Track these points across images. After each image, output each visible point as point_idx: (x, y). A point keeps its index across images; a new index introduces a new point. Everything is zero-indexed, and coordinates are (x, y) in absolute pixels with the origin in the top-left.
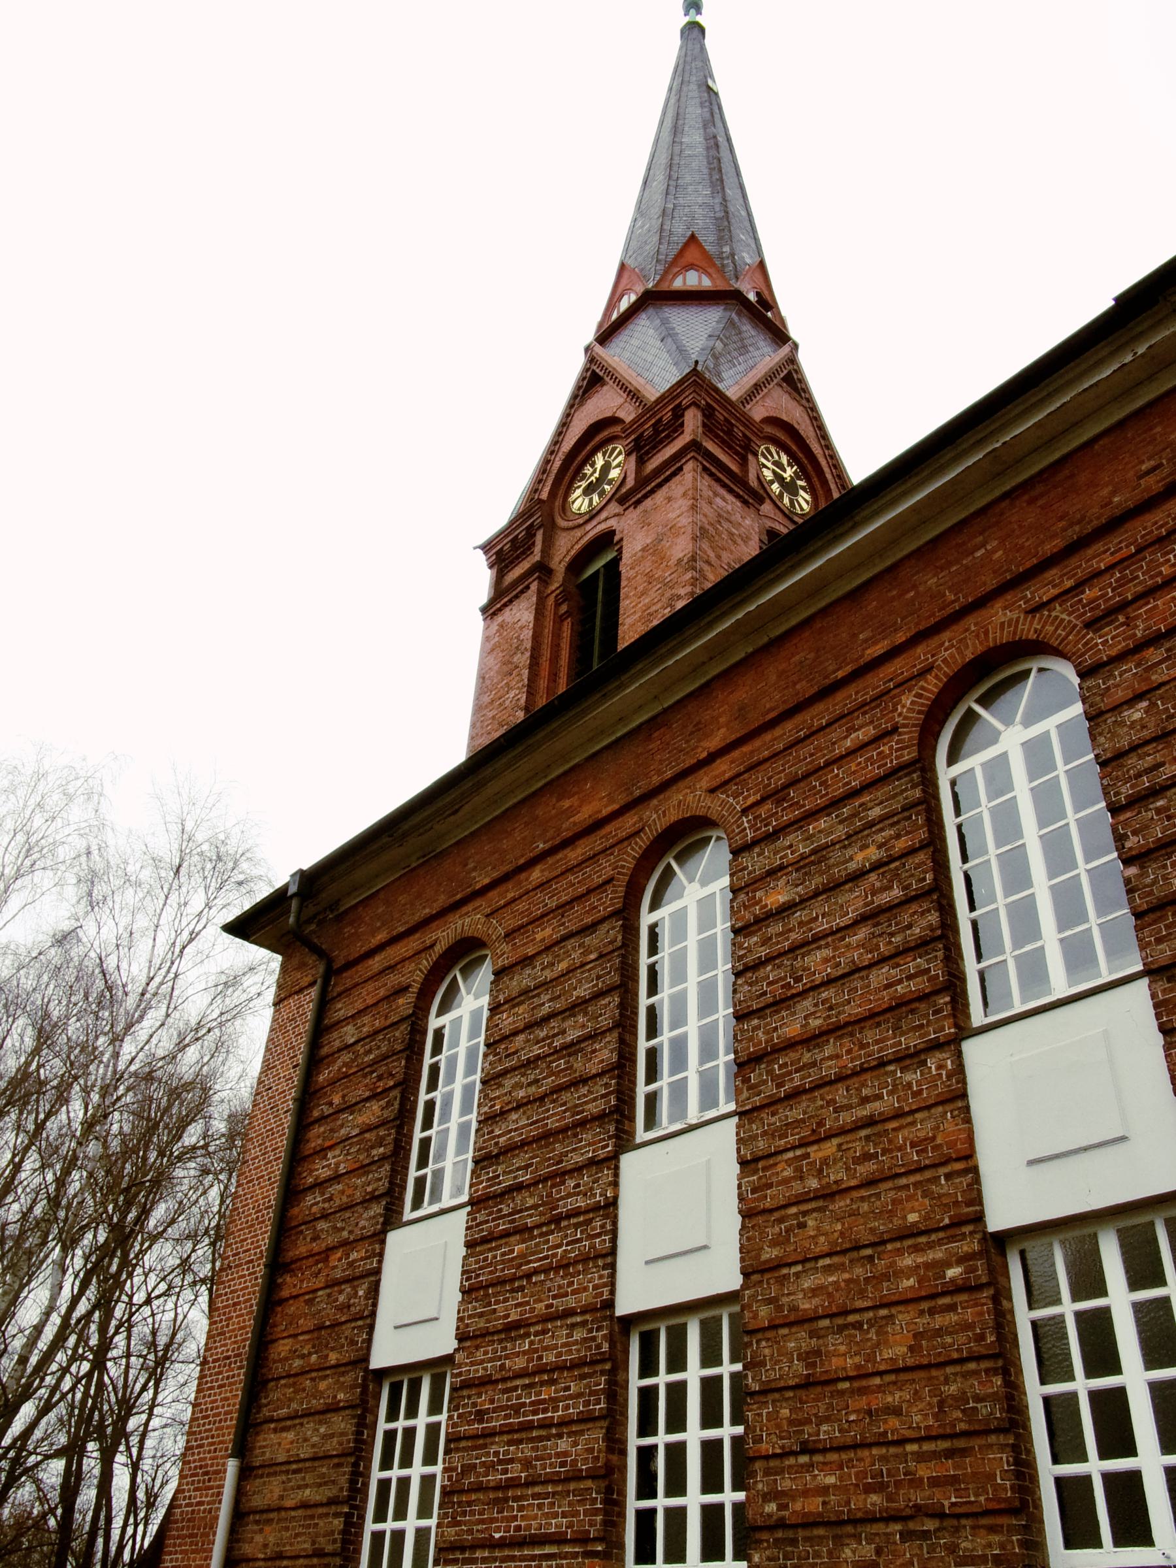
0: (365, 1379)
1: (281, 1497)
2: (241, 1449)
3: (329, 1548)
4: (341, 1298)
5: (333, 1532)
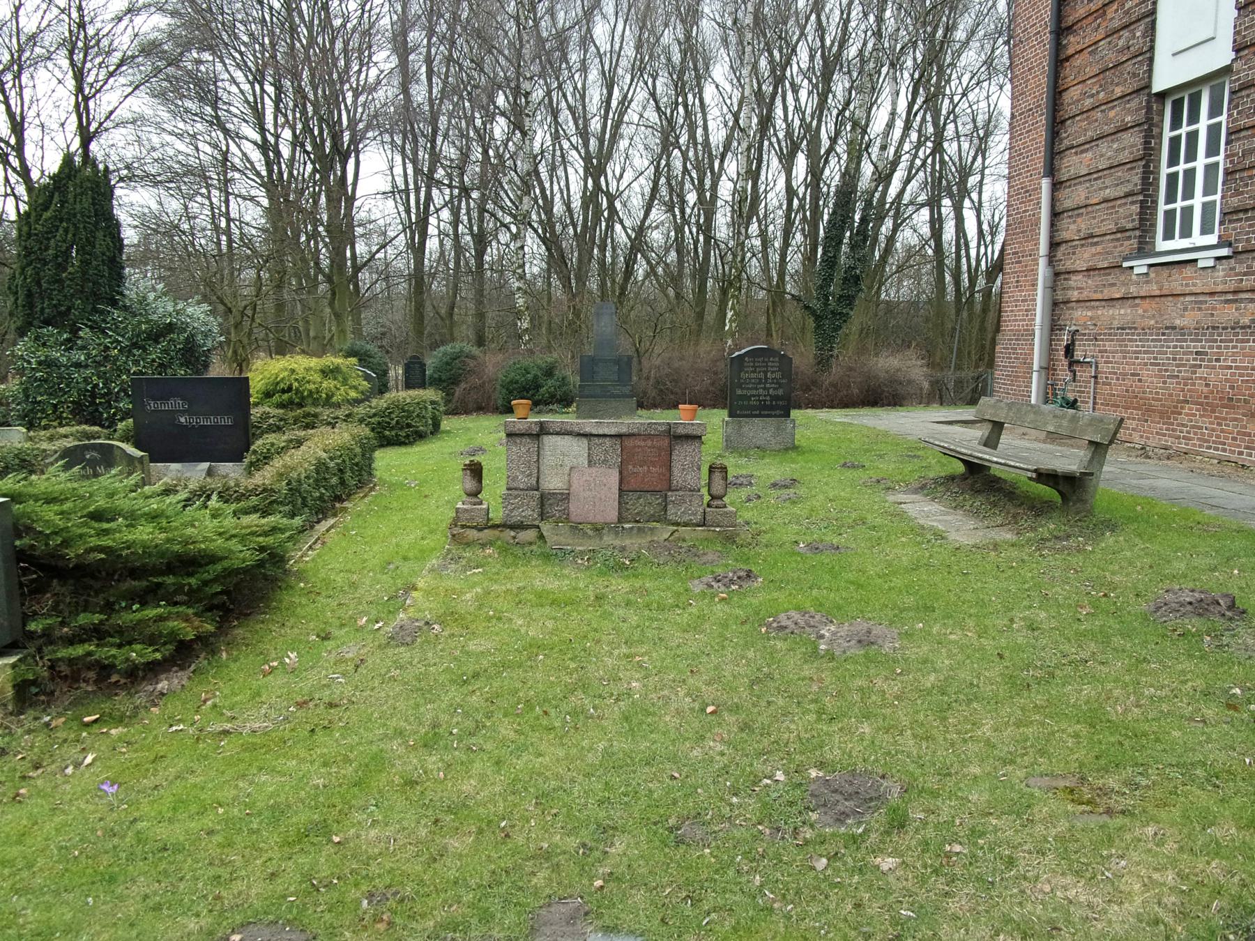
0: (1148, 102)
1: (1087, 198)
2: (1051, 170)
3: (1130, 226)
4: (1121, 43)
5: (1131, 215)
